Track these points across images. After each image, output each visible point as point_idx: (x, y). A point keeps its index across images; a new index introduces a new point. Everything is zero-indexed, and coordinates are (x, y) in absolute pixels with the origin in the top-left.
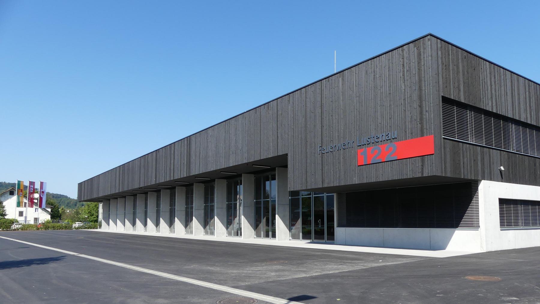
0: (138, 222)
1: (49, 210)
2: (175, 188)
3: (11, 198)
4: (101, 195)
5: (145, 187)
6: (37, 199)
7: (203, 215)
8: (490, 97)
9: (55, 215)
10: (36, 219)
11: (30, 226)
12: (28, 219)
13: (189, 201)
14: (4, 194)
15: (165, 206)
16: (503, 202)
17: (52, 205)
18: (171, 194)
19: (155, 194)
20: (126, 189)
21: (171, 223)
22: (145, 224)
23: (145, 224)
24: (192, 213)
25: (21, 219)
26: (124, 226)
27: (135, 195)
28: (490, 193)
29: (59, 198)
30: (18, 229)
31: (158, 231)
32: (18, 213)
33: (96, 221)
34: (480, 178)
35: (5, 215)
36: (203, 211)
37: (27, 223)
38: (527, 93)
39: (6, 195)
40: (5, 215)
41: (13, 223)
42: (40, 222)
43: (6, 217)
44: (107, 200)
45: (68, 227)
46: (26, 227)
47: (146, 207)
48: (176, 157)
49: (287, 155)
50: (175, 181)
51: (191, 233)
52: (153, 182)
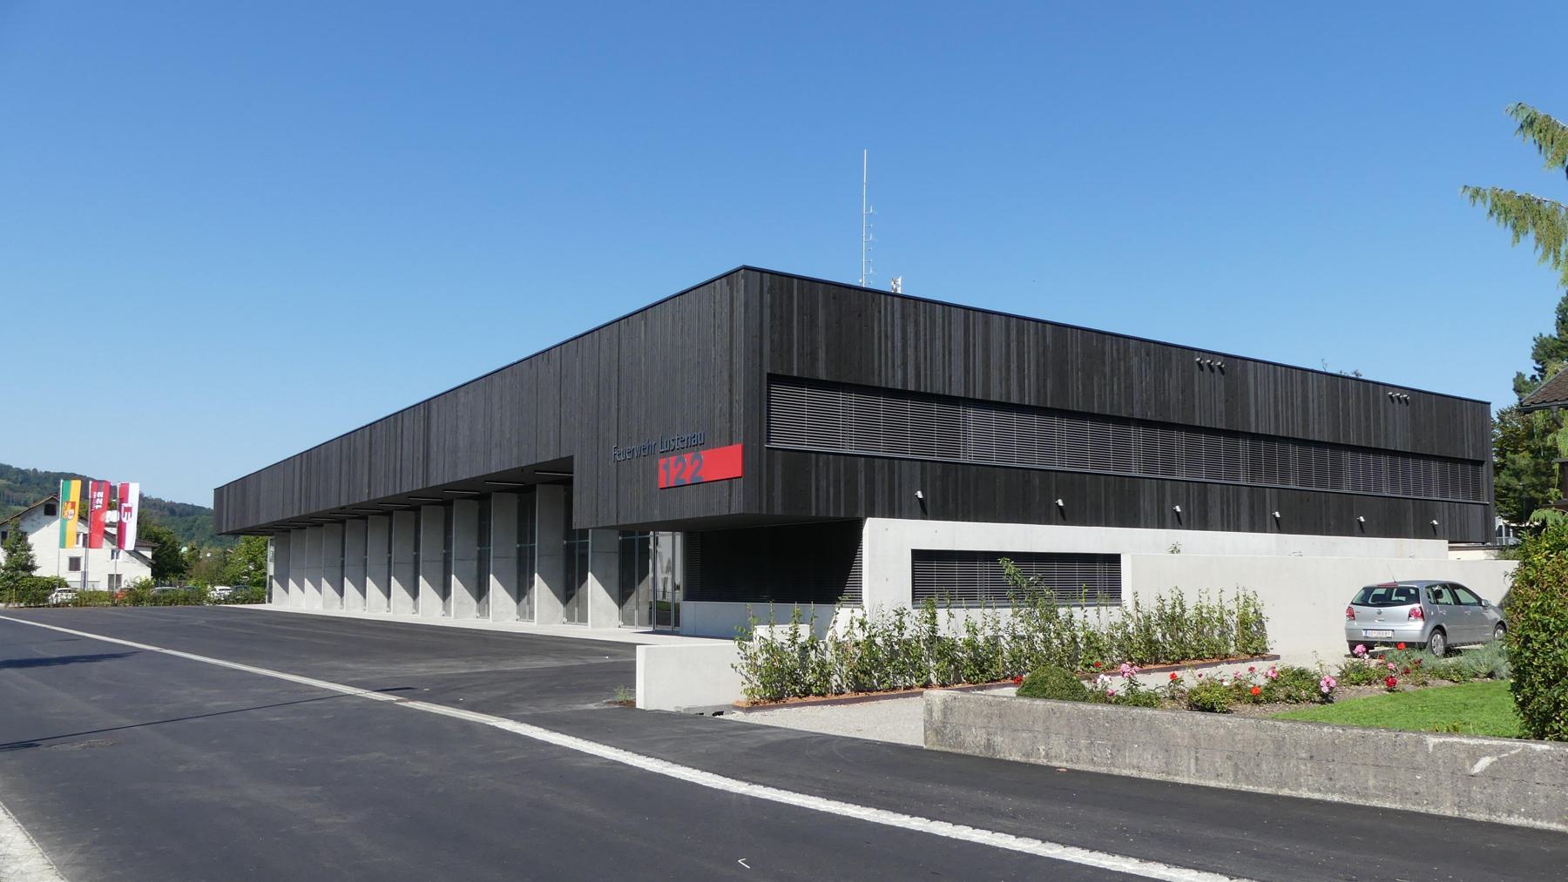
0: (349, 586)
1: (149, 554)
2: (532, 488)
3: (49, 523)
4: (264, 520)
5: (444, 487)
6: (111, 525)
7: (474, 573)
8: (898, 361)
9: (165, 565)
10: (115, 579)
11: (96, 596)
12: (90, 578)
13: (525, 532)
14: (29, 512)
15: (402, 549)
16: (919, 556)
17: (157, 539)
18: (480, 511)
19: (474, 506)
20: (313, 510)
21: (521, 591)
22: (445, 593)
23: (445, 593)
24: (584, 557)
25: (73, 578)
26: (388, 596)
27: (447, 504)
28: (888, 545)
29: (188, 514)
30: (65, 604)
31: (483, 611)
32: (66, 563)
33: (262, 583)
34: (861, 514)
35: (33, 568)
36: (475, 564)
37: (89, 588)
38: (1013, 345)
39: (35, 517)
40: (33, 568)
41: (54, 588)
42: (123, 586)
43: (34, 573)
44: (282, 531)
45: (199, 597)
46: (86, 599)
47: (447, 544)
48: (405, 443)
49: (572, 458)
50: (537, 468)
51: (583, 619)
52: (363, 497)
